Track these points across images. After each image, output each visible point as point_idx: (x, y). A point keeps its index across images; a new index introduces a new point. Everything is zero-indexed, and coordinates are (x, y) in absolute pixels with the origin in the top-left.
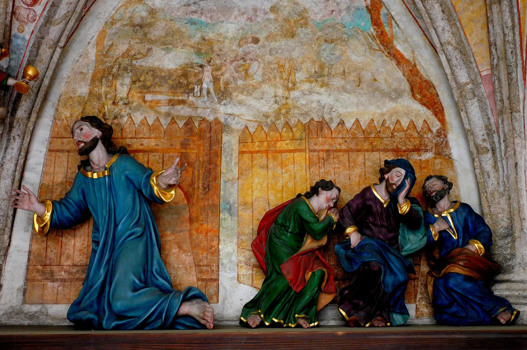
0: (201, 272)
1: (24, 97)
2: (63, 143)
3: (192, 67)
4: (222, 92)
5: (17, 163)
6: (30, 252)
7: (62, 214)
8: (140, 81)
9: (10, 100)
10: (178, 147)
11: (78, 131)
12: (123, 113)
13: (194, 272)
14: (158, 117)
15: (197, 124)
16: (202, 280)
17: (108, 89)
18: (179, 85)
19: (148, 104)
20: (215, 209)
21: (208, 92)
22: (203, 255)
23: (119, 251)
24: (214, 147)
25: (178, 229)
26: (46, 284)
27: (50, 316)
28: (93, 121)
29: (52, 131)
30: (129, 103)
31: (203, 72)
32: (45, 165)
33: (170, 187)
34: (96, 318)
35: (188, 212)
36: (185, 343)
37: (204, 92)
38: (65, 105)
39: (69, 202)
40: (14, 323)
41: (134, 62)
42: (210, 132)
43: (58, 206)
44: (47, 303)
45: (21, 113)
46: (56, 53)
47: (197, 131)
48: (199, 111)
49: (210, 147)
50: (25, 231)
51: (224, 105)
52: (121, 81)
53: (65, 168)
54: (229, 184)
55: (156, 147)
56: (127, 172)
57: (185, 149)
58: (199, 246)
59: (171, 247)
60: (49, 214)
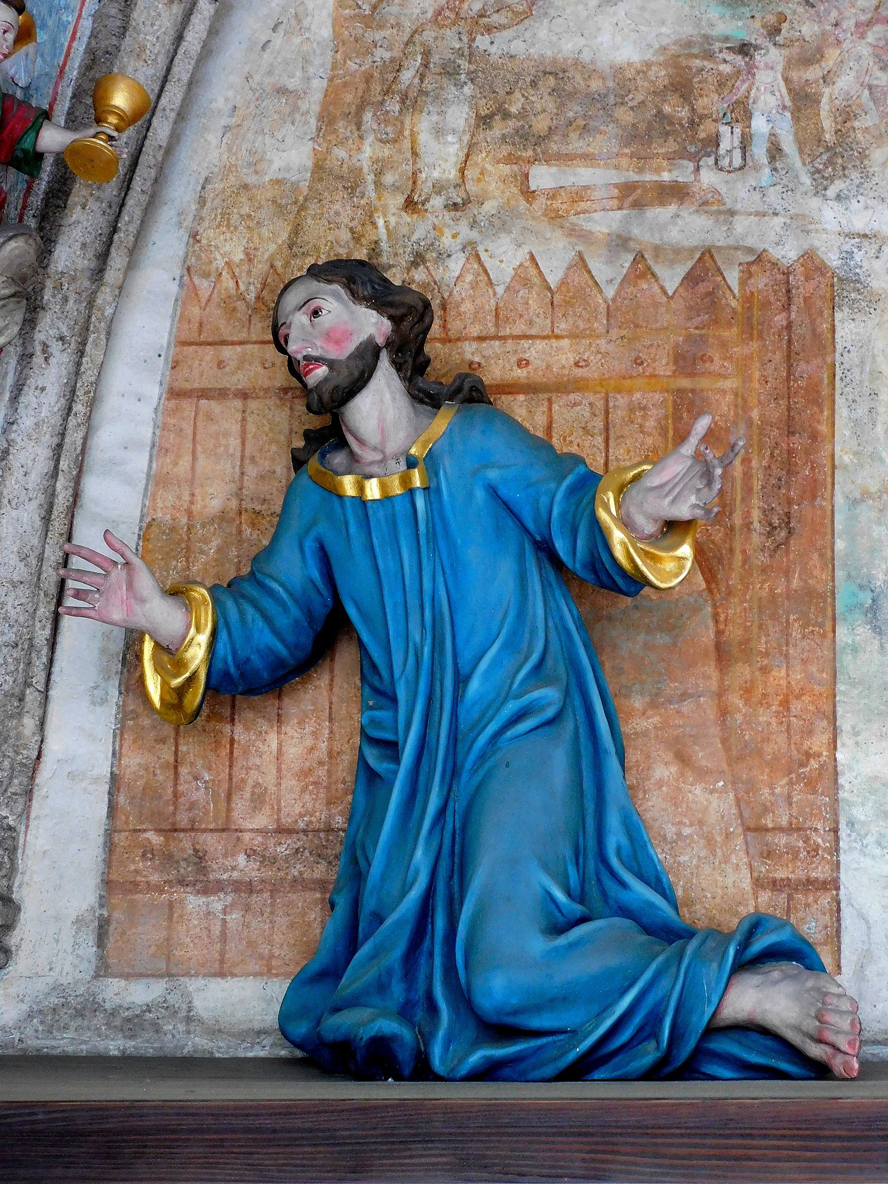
0: (769, 854)
1: (79, 192)
2: (221, 365)
3: (709, 55)
4: (828, 149)
5: (60, 446)
6: (115, 780)
7: (248, 638)
8: (506, 115)
9: (24, 207)
10: (663, 367)
11: (301, 319)
12: (447, 241)
13: (742, 854)
14: (580, 255)
15: (733, 277)
16: (775, 885)
17: (386, 151)
18: (663, 125)
19: (540, 203)
20: (817, 608)
21: (775, 152)
22: (773, 789)
23: (478, 778)
24: (802, 367)
25: (672, 687)
26: (181, 901)
27: (201, 1021)
28: (359, 277)
29: (181, 318)
30: (467, 202)
31: (751, 70)
32: (158, 449)
33: (673, 528)
34: (406, 1034)
35: (711, 624)
36: (794, 1137)
37: (759, 151)
38: (226, 216)
39: (270, 592)
40: (70, 1049)
41: (482, 42)
42: (787, 307)
43: (230, 605)
44: (187, 974)
45: (70, 253)
46: (195, 20)
47: (734, 303)
48: (741, 224)
49: (790, 366)
50: (93, 703)
51: (838, 198)
52: (435, 118)
53: (239, 458)
54: (866, 512)
55: (579, 372)
56: (493, 475)
57: (692, 375)
58: (760, 753)
59: (648, 757)
60: (203, 639)
